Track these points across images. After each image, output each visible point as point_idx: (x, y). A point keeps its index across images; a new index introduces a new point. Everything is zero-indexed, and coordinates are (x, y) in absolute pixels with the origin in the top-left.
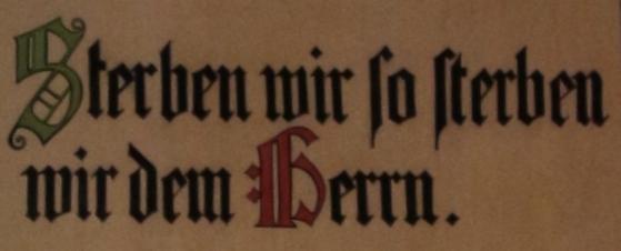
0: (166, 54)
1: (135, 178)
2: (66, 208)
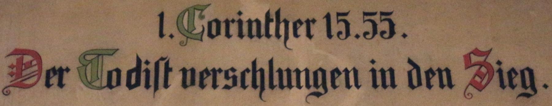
1: (410, 74)
2: (315, 73)
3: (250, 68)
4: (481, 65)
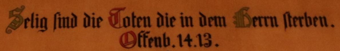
0: (305, 14)
3: (30, 18)
4: (17, 16)
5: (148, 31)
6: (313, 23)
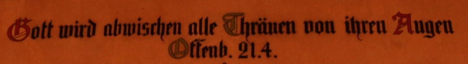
5: (204, 39)
6: (314, 29)
